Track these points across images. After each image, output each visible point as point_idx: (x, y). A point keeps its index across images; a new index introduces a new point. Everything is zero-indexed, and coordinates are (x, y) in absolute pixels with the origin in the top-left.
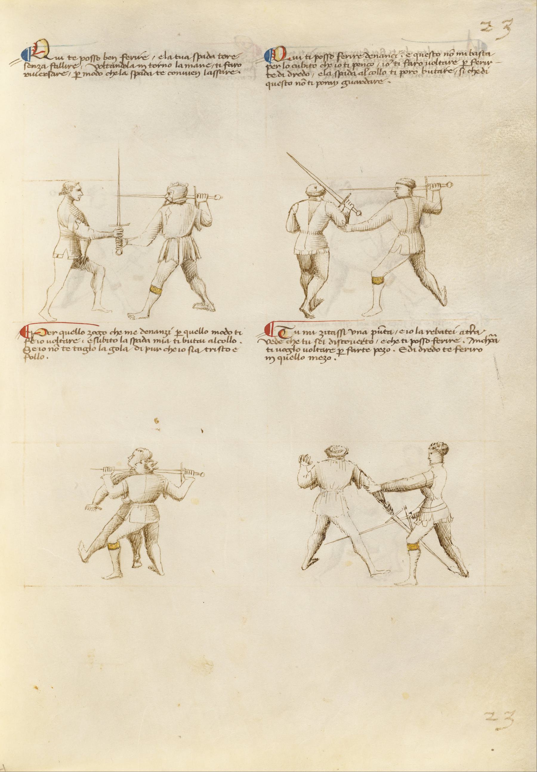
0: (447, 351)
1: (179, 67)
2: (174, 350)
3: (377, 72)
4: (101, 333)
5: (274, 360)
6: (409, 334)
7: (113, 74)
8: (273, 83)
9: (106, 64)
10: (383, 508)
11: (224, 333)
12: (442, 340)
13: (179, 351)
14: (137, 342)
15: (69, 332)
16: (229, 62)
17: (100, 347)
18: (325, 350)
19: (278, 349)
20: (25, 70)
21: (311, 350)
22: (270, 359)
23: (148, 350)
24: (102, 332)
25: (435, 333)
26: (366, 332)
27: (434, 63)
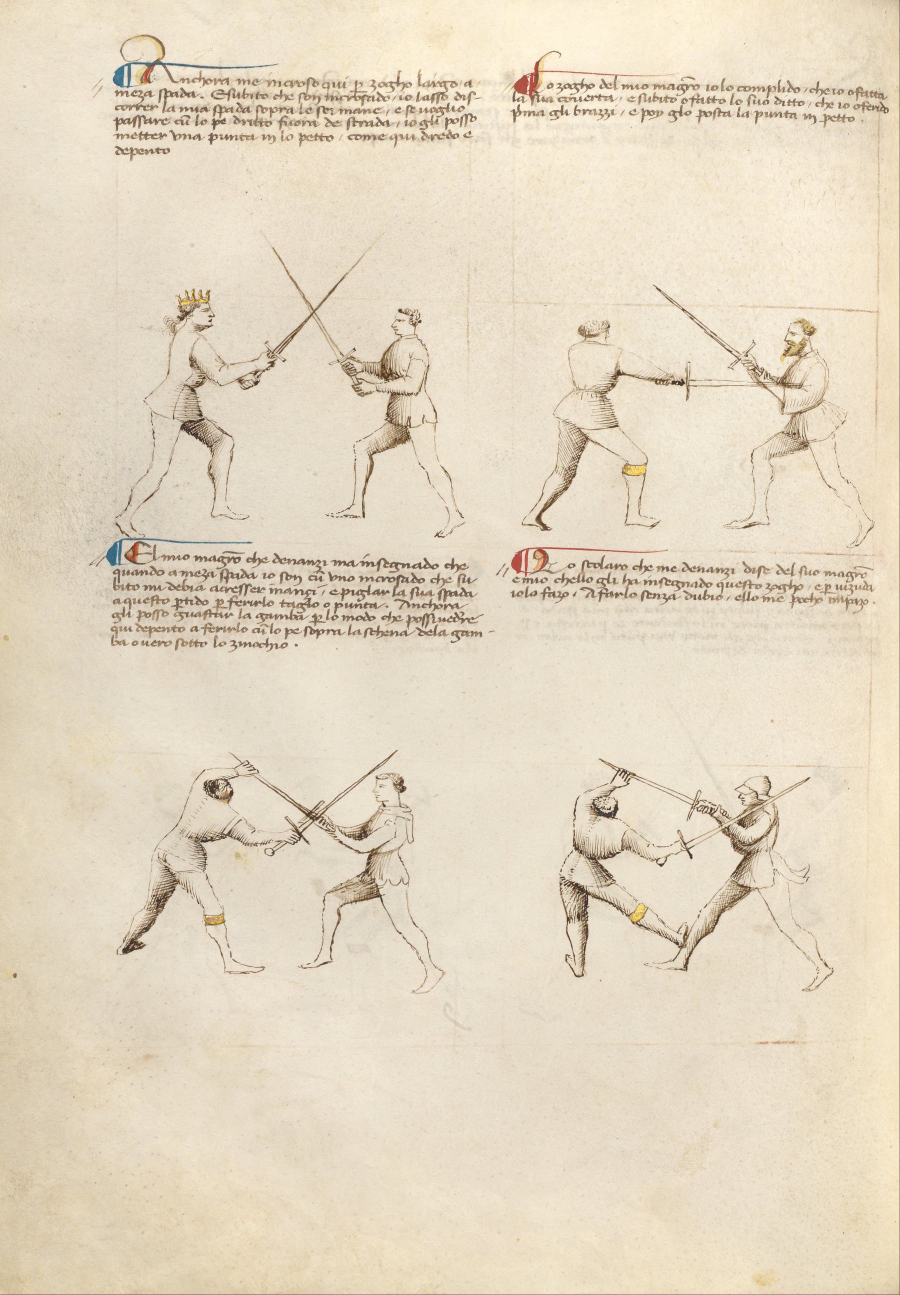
0: (162, 153)
4: (680, 585)
6: (408, 127)
11: (363, 618)
12: (159, 642)
16: (868, 103)
19: (653, 583)
26: (624, 86)
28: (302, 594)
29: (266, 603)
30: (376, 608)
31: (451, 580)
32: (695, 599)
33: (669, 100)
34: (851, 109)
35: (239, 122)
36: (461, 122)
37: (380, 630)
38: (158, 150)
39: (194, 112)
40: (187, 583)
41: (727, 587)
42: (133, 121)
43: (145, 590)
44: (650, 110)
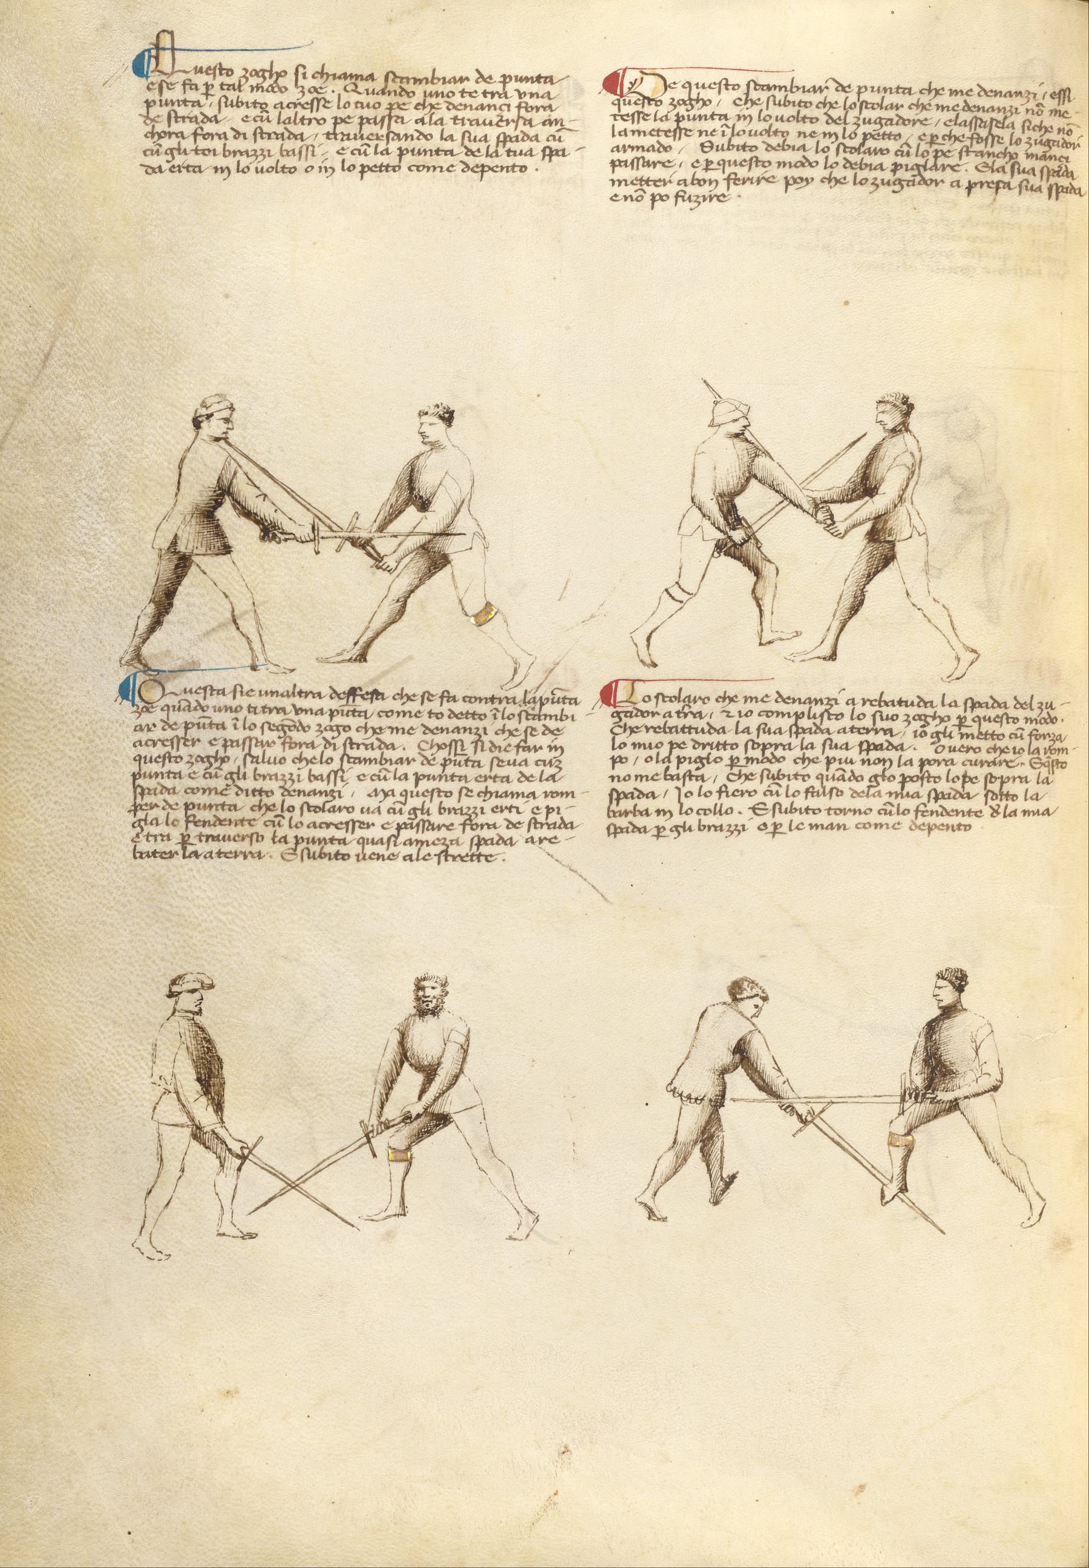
2: (974, 780)
13: (260, 695)
14: (511, 141)
15: (650, 744)
17: (280, 116)
20: (270, 60)
27: (764, 133)
29: (995, 168)
30: (452, 155)
33: (962, 828)
34: (304, 828)
36: (450, 749)
37: (155, 131)
42: (633, 164)
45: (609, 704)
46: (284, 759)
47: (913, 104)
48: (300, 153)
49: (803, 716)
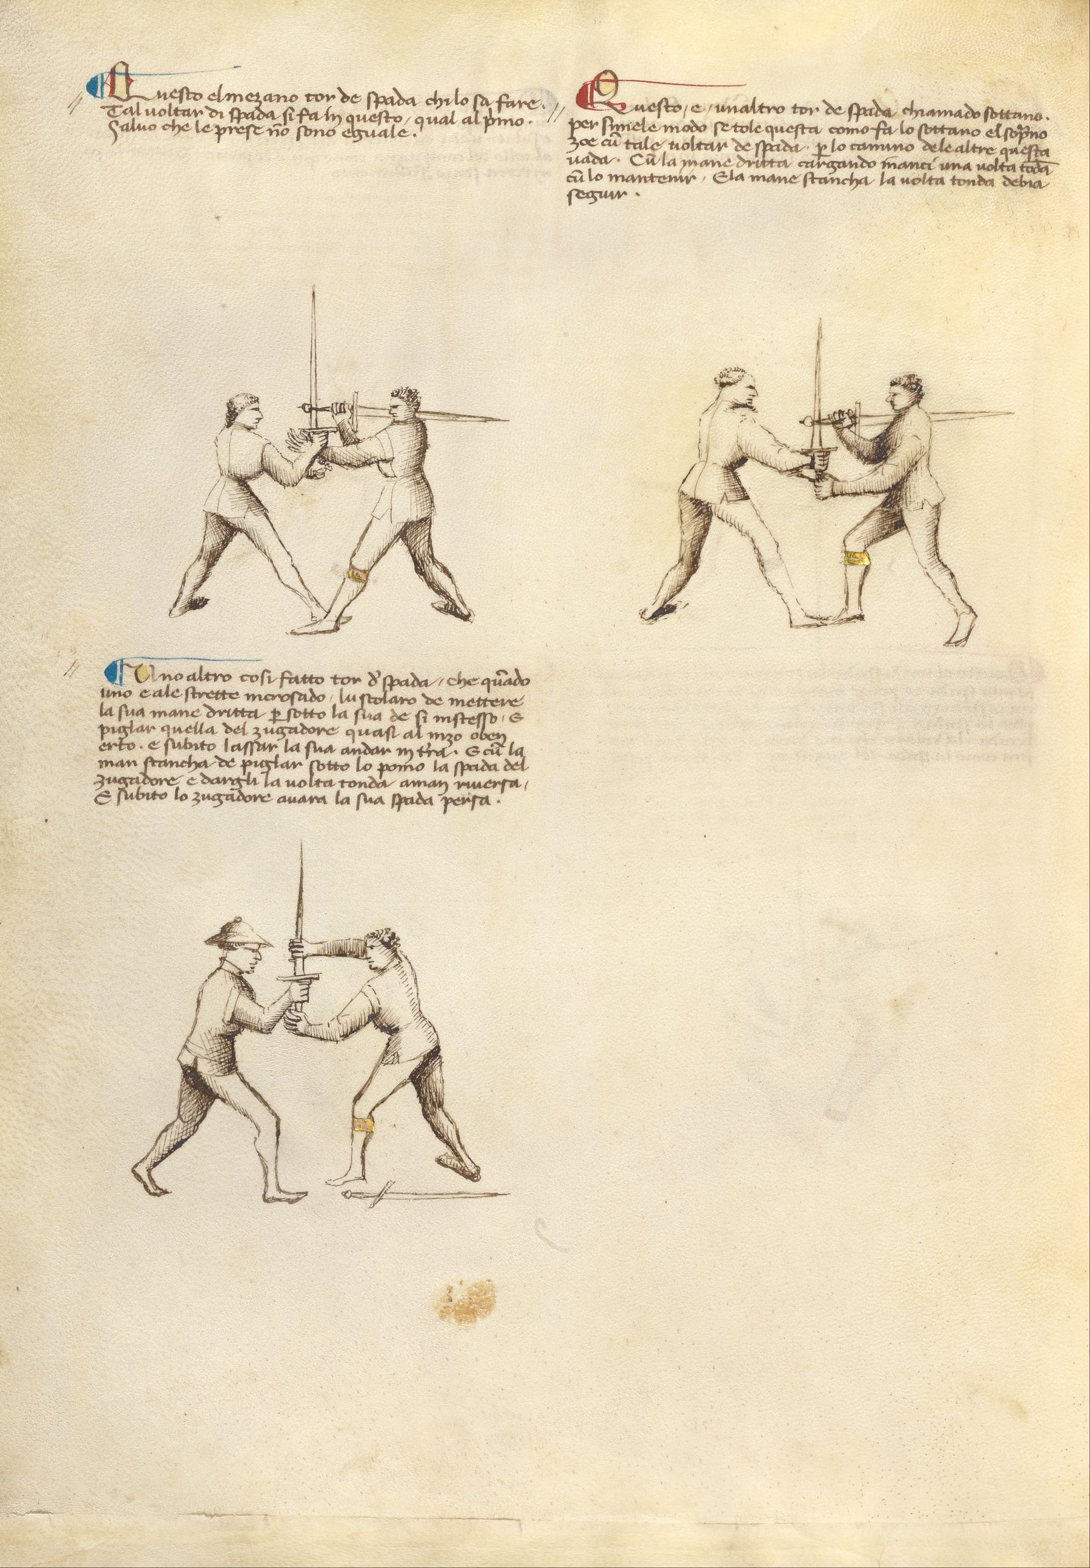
1: (342, 803)
3: (308, 783)
4: (836, 165)
5: (340, 121)
7: (462, 683)
8: (713, 143)
9: (696, 142)
10: (354, 142)
18: (266, 746)
21: (162, 113)
22: (334, 119)
23: (489, 125)
24: (857, 145)
25: (641, 127)
28: (285, 101)
31: (199, 714)
32: (148, 799)
35: (214, 713)
37: (854, 178)
38: (652, 177)
39: (259, 767)
40: (141, 791)
41: (495, 684)
43: (399, 755)
44: (370, 755)
45: (95, 95)
46: (155, 126)
47: (167, 125)
48: (455, 719)
49: (265, 97)
